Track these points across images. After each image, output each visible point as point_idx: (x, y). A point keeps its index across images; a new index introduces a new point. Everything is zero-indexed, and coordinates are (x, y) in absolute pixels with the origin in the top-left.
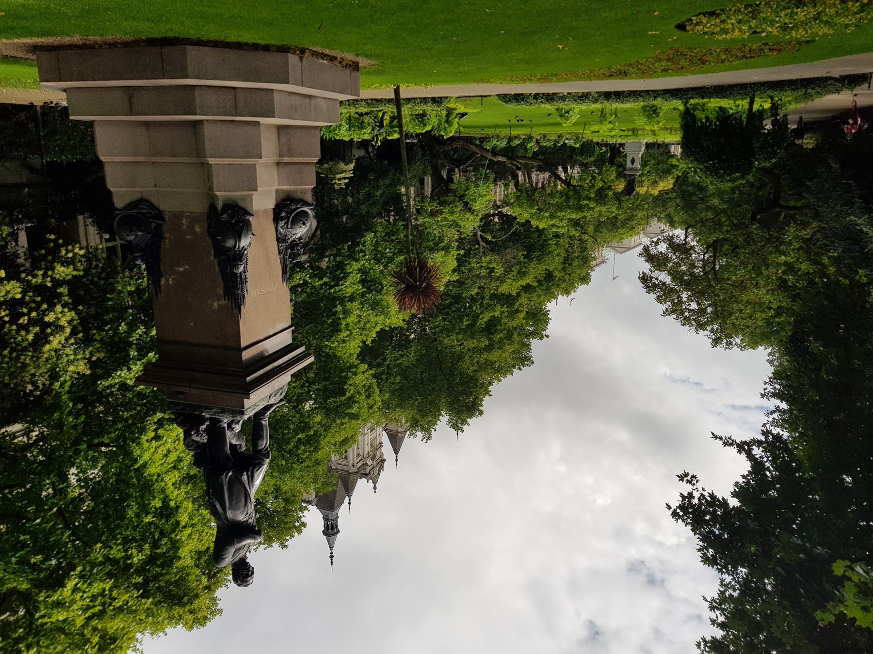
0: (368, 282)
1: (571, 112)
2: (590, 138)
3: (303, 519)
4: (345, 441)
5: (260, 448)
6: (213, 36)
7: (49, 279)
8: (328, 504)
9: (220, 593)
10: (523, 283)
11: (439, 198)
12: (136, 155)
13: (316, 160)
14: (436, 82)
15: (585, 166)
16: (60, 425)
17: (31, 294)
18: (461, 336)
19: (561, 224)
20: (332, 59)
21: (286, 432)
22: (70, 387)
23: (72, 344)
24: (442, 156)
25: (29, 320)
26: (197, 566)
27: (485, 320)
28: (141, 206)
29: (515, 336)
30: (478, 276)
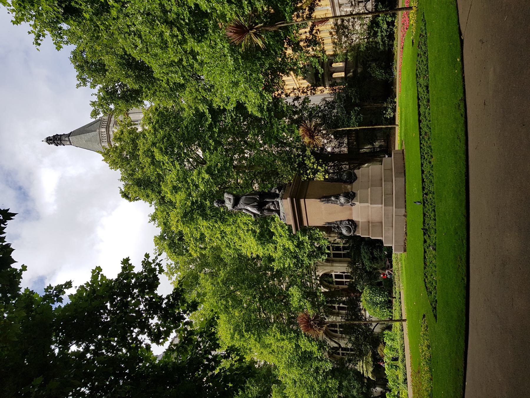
12: (371, 176)
14: (409, 338)
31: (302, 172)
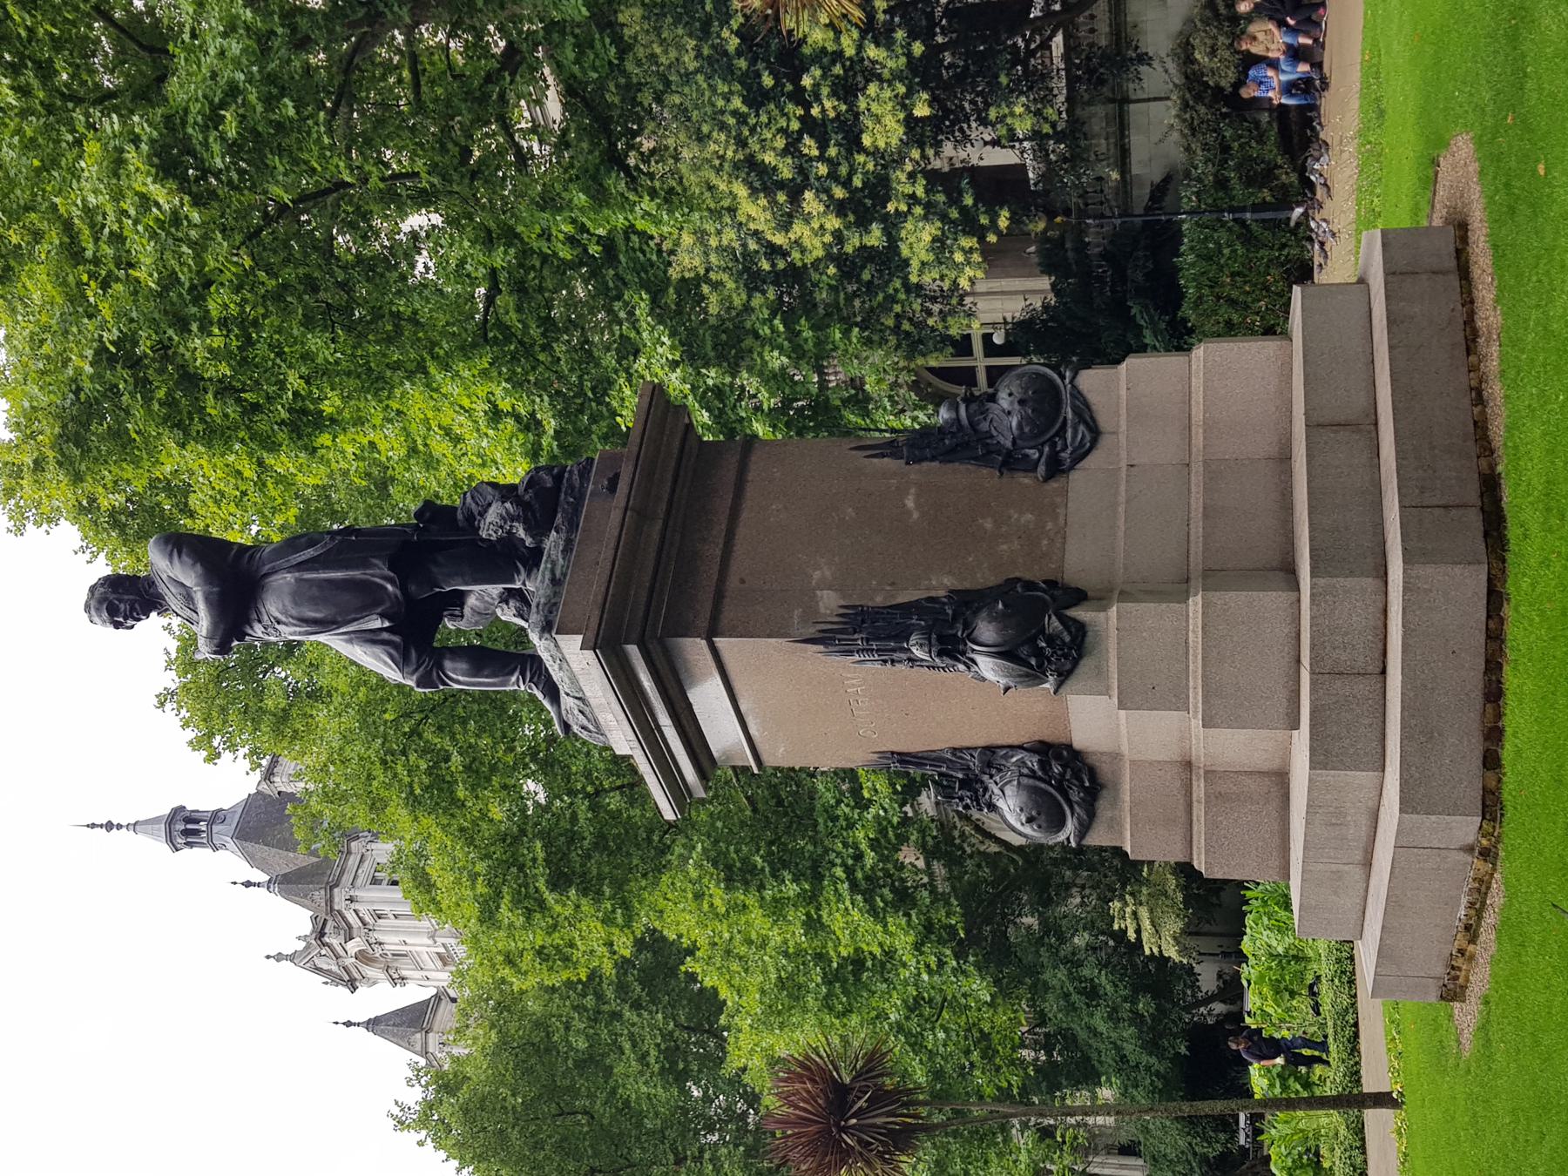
3: (227, 756)
4: (423, 883)
5: (448, 664)
6: (1516, 633)
7: (903, 208)
8: (259, 825)
9: (68, 533)
12: (1208, 427)
13: (1199, 864)
16: (549, 202)
17: (870, 166)
20: (1471, 931)
23: (744, 245)
25: (811, 159)
26: (153, 484)
28: (1082, 428)
31: (768, 81)
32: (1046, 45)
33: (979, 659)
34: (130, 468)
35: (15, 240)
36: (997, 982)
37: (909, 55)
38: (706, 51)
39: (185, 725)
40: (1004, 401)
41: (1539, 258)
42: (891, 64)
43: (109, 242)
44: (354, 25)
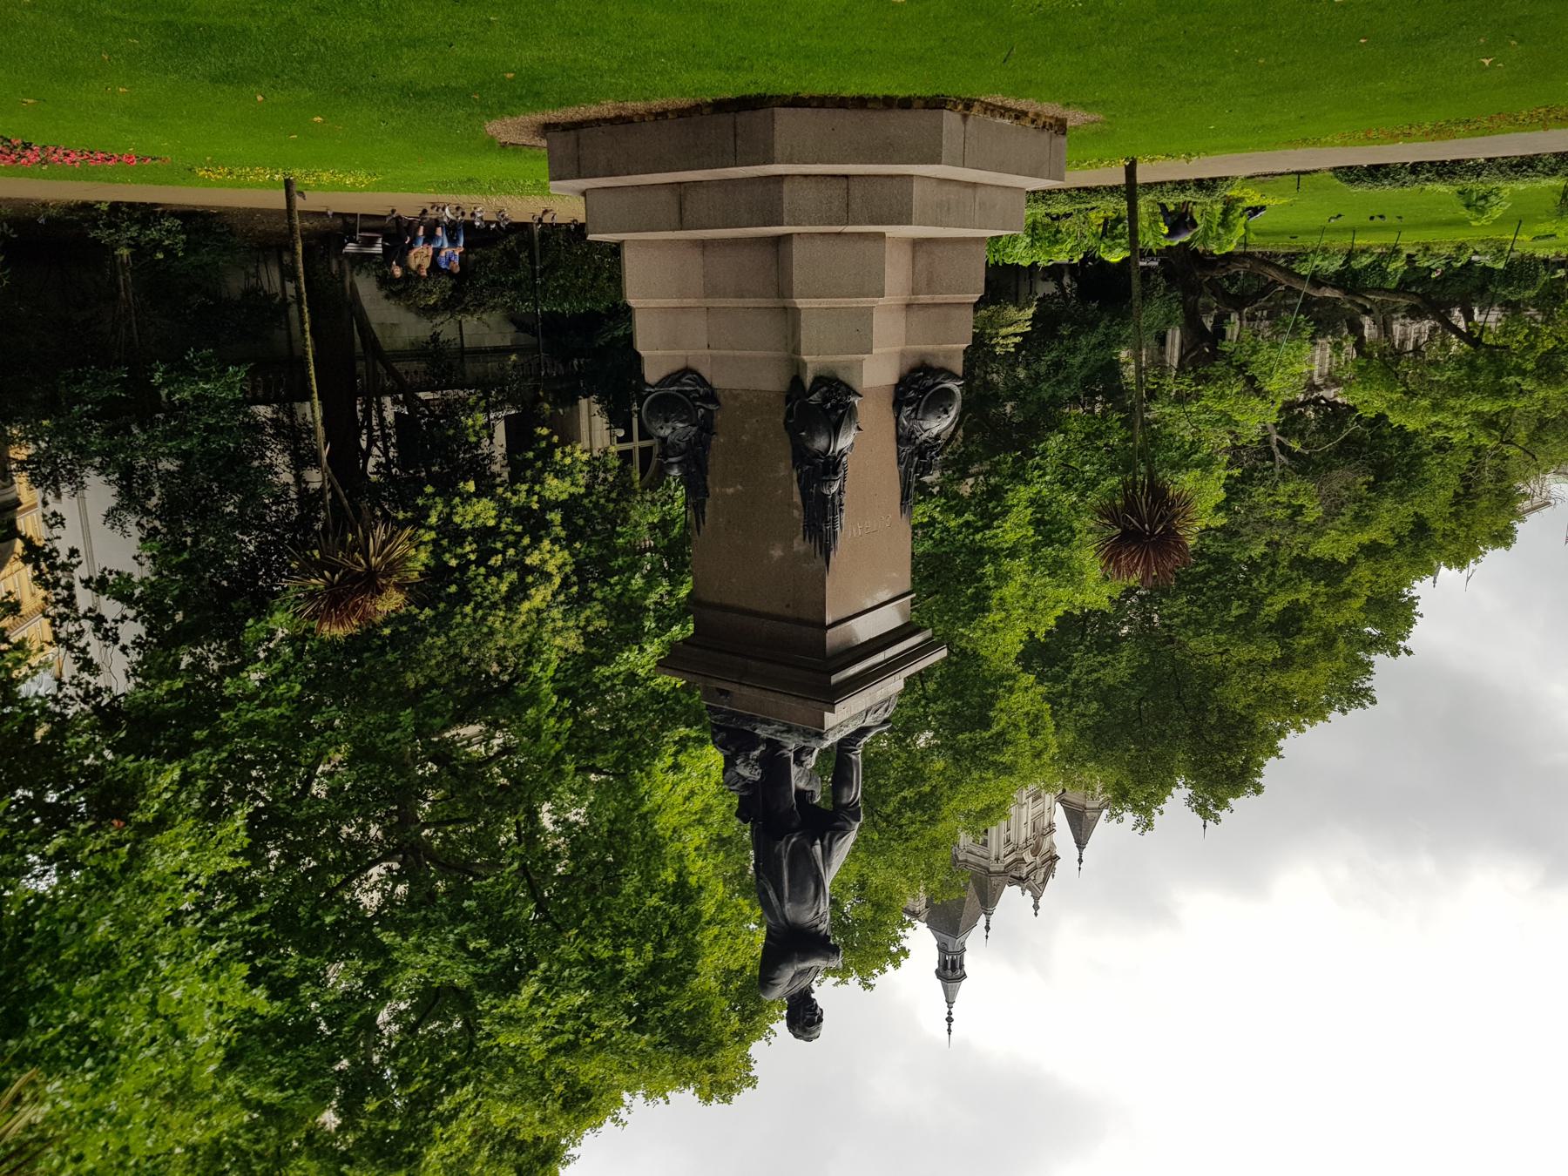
0: (1045, 523)
1: (1492, 199)
2: (1530, 250)
3: (904, 943)
4: (986, 813)
5: (845, 801)
7: (535, 498)
8: (950, 923)
9: (757, 1049)
10: (1364, 538)
11: (1195, 370)
12: (682, 296)
13: (975, 298)
15: (1512, 308)
16: (535, 733)
17: (508, 520)
18: (1224, 637)
19: (1456, 423)
20: (1019, 115)
21: (882, 781)
22: (556, 671)
23: (562, 603)
24: (1206, 289)
25: (504, 560)
26: (723, 994)
27: (1278, 607)
29: (1341, 644)
30: (1268, 522)
31: (453, 589)
32: (426, 403)
33: (839, 448)
34: (713, 1010)
35: (561, 1087)
36: (1051, 429)
37: (434, 495)
38: (434, 630)
39: (884, 971)
40: (666, 432)
41: (569, 77)
42: (440, 507)
43: (563, 1024)
44: (420, 864)
